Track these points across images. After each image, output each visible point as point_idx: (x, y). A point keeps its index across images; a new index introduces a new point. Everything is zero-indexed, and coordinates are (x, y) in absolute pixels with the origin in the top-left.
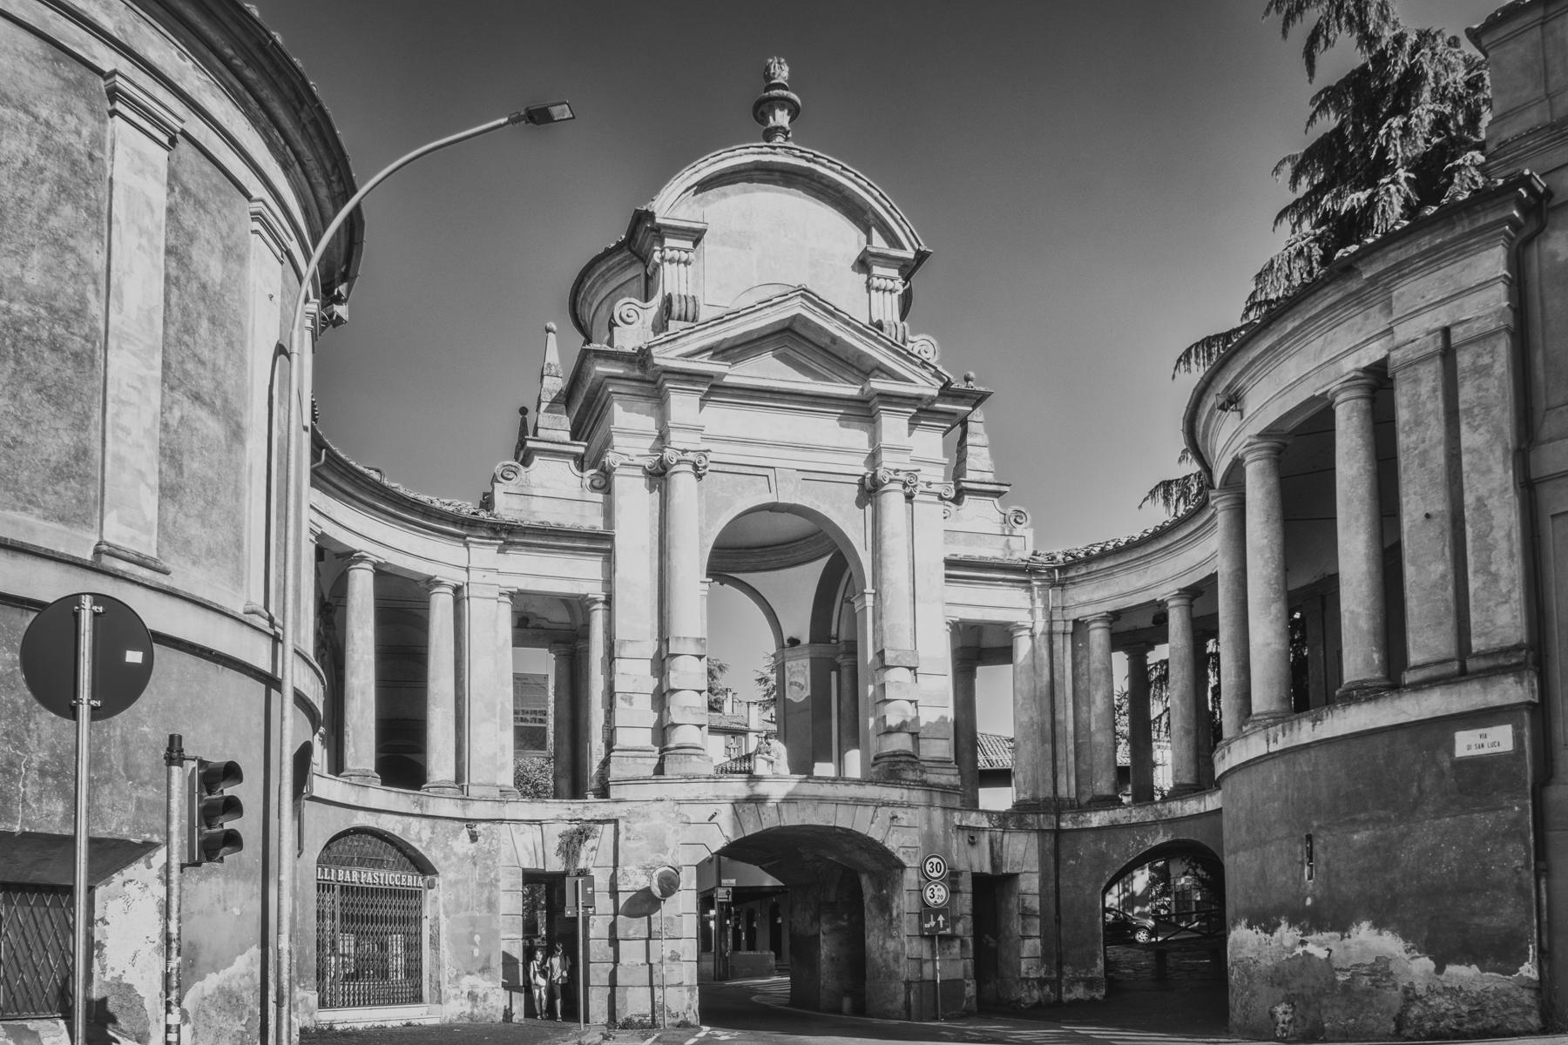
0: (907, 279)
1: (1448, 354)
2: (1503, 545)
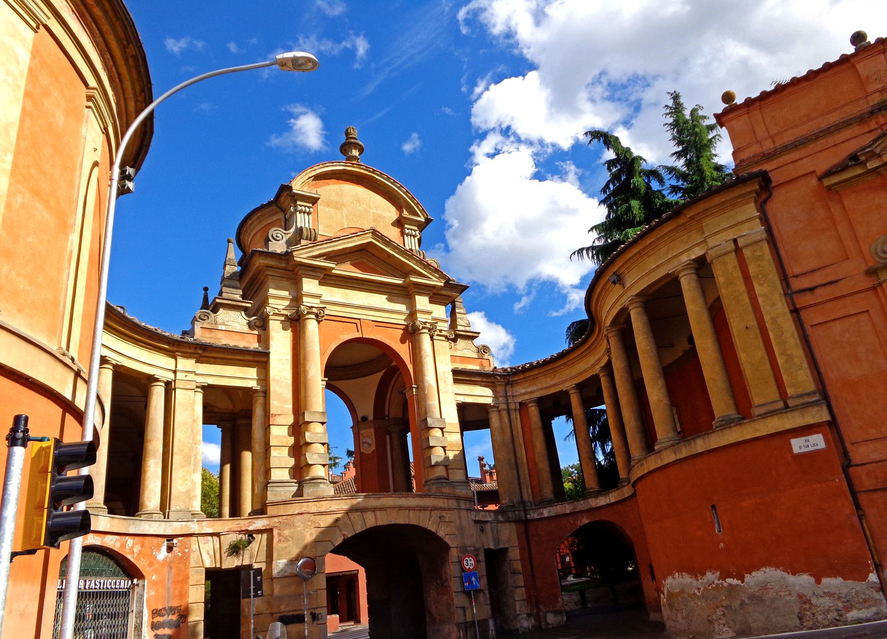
0: (421, 231)
1: (738, 251)
2: (791, 341)
